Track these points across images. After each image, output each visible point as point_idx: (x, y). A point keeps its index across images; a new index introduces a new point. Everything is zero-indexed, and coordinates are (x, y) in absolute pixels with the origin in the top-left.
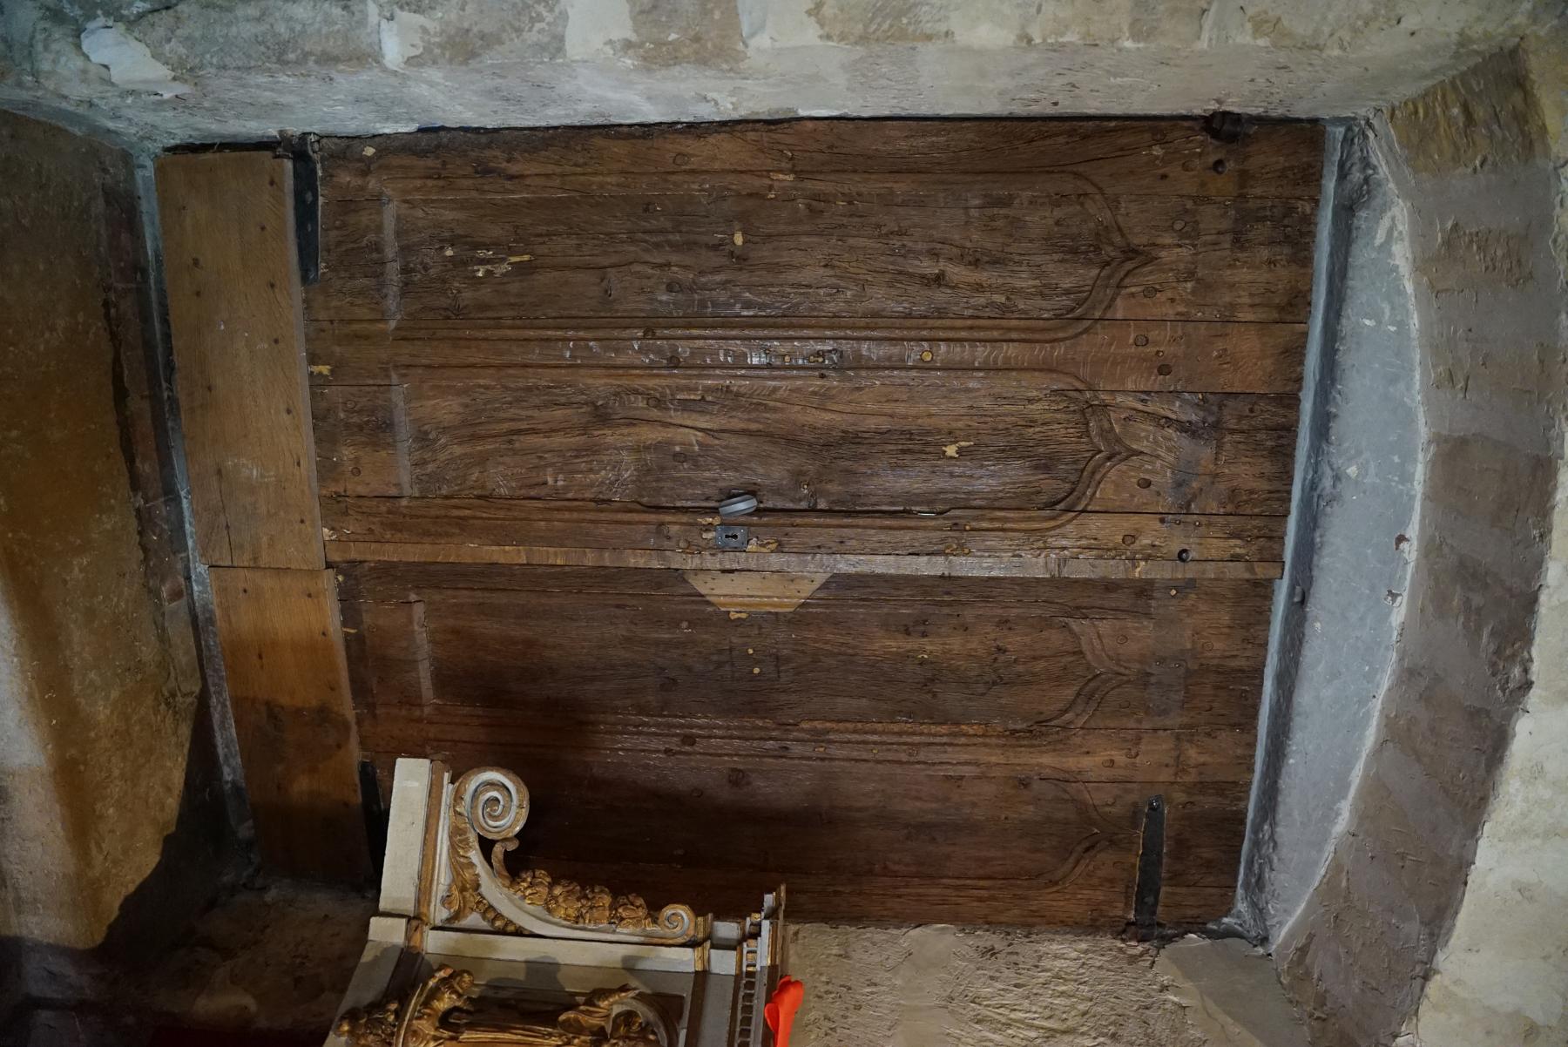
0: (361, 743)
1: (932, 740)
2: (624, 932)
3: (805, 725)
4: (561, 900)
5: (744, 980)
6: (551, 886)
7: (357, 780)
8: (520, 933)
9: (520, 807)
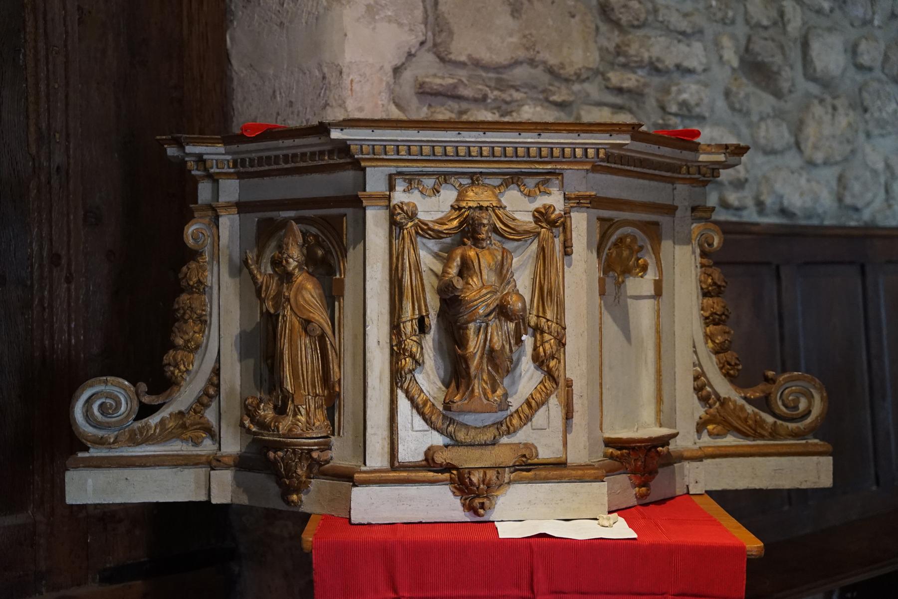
0: (79, 585)
1: (41, 31)
2: (210, 279)
3: (33, 150)
4: (186, 337)
5: (243, 171)
6: (175, 347)
7: (114, 587)
8: (217, 371)
9: (106, 382)
